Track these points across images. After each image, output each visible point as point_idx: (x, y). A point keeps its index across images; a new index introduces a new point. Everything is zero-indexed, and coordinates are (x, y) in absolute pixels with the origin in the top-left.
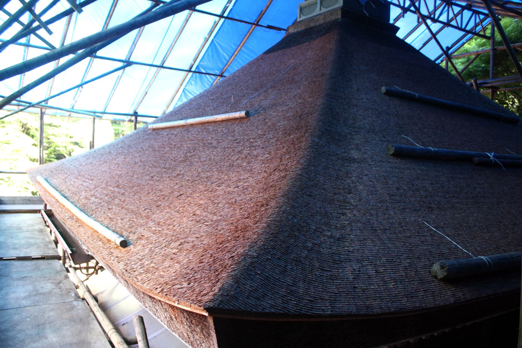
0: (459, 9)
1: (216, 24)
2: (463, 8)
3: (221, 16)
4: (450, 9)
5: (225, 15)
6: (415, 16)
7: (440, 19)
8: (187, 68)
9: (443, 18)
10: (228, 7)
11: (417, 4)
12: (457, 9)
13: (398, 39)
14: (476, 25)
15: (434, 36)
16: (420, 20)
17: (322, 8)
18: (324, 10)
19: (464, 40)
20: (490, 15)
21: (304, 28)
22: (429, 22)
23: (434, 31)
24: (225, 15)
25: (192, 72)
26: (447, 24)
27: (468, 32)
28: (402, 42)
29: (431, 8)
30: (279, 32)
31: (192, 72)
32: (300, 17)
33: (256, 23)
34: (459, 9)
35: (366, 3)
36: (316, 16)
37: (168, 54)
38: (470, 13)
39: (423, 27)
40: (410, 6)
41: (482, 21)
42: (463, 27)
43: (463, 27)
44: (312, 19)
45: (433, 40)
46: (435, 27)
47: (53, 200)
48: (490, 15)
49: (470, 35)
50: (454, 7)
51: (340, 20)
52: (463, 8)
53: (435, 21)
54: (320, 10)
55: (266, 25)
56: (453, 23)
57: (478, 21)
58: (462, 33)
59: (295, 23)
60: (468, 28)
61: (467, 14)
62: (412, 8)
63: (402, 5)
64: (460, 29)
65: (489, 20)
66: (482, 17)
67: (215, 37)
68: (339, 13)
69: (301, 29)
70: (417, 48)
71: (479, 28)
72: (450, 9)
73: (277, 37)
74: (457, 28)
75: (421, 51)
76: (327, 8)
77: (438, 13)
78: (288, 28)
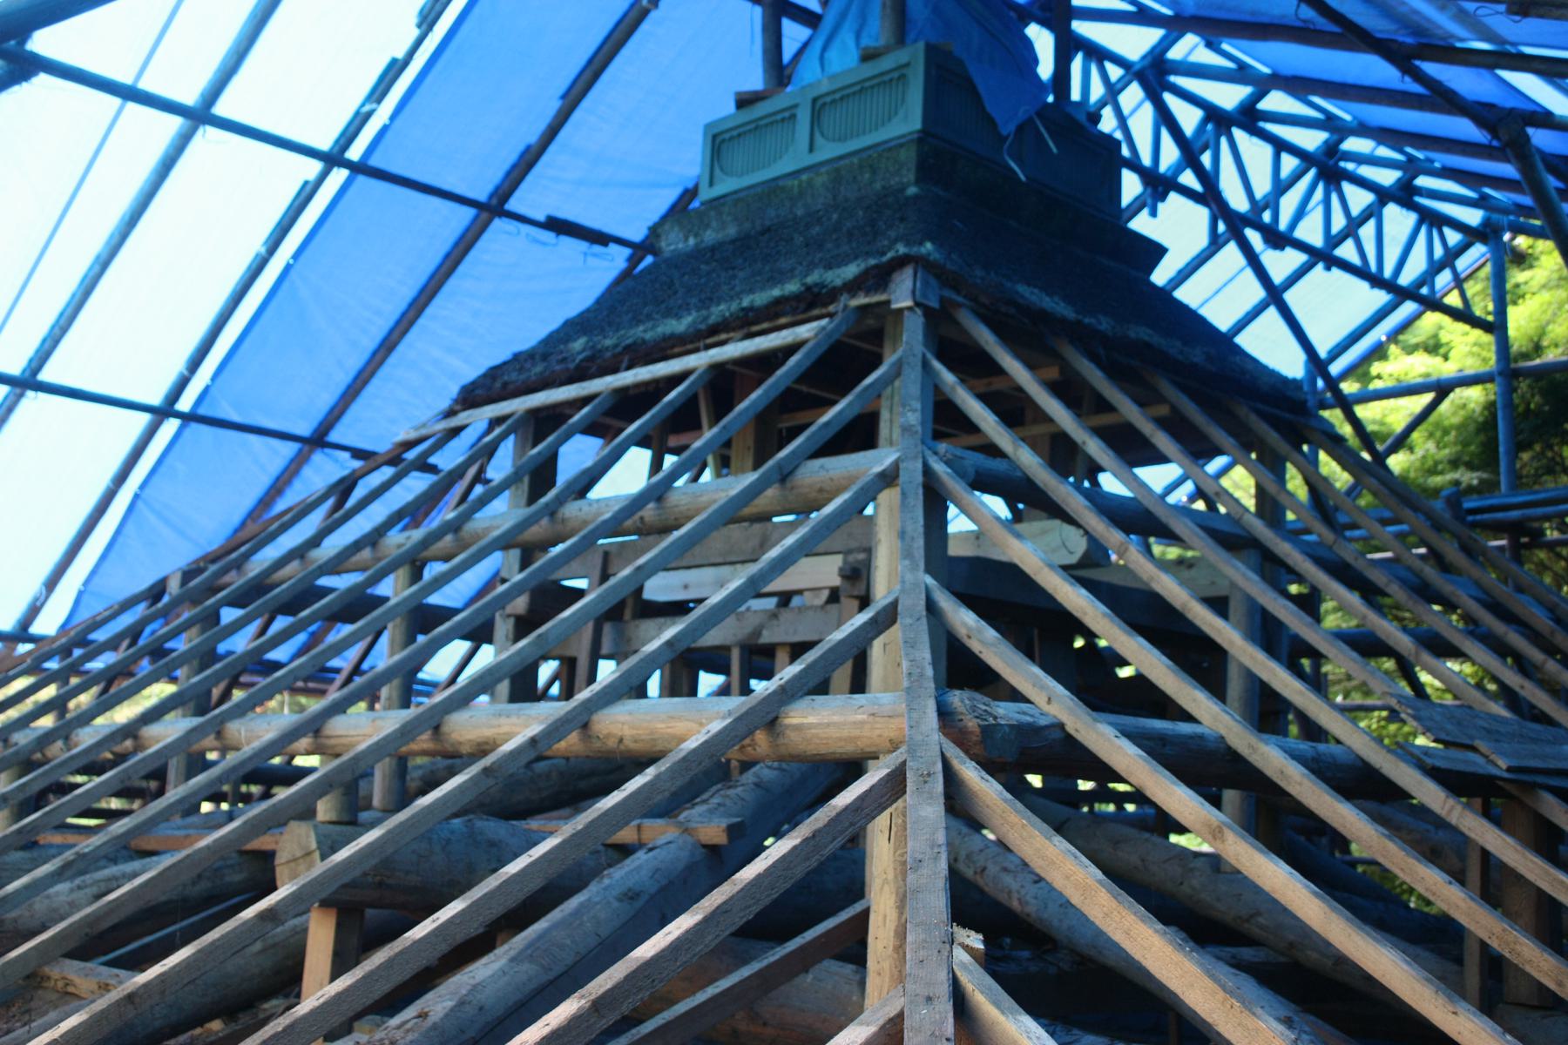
0: (1367, 198)
1: (306, 194)
2: (1384, 196)
3: (332, 159)
4: (1334, 197)
5: (354, 153)
6: (1202, 214)
7: (1299, 234)
8: (156, 399)
9: (1311, 231)
10: (369, 115)
11: (1206, 159)
12: (1359, 199)
13: (1154, 286)
14: (1435, 268)
15: (1275, 295)
16: (1221, 227)
17: (819, 140)
18: (828, 150)
19: (1379, 333)
20: (1524, 185)
21: (732, 231)
22: (1254, 237)
23: (1278, 277)
24: (354, 153)
25: (178, 415)
26: (1323, 256)
27: (1402, 294)
28: (1164, 296)
29: (1262, 187)
30: (597, 248)
31: (178, 415)
32: (711, 184)
33: (494, 201)
34: (1367, 198)
35: (1020, 129)
36: (795, 174)
37: (588, 74)
38: (1411, 218)
39: (1231, 254)
40: (1179, 170)
41: (1452, 255)
42: (1388, 273)
43: (1388, 273)
44: (772, 189)
45: (1272, 313)
46: (1281, 263)
47: (804, 177)
48: (1524, 185)
49: (1409, 307)
50: (1347, 187)
51: (912, 190)
52: (1384, 196)
53: (1277, 240)
54: (811, 149)
55: (540, 216)
56: (1347, 251)
57: (1439, 252)
58: (1382, 297)
59: (680, 209)
60: (1405, 279)
61: (1398, 220)
62: (1188, 179)
63: (1146, 160)
64: (1376, 281)
65: (1478, 251)
66: (1453, 237)
67: (297, 255)
68: (909, 156)
69: (720, 236)
70: (1223, 323)
71: (1444, 279)
72: (1334, 197)
73: (586, 277)
74: (1361, 272)
75: (1243, 340)
76: (842, 139)
77: (1289, 203)
78: (654, 231)
